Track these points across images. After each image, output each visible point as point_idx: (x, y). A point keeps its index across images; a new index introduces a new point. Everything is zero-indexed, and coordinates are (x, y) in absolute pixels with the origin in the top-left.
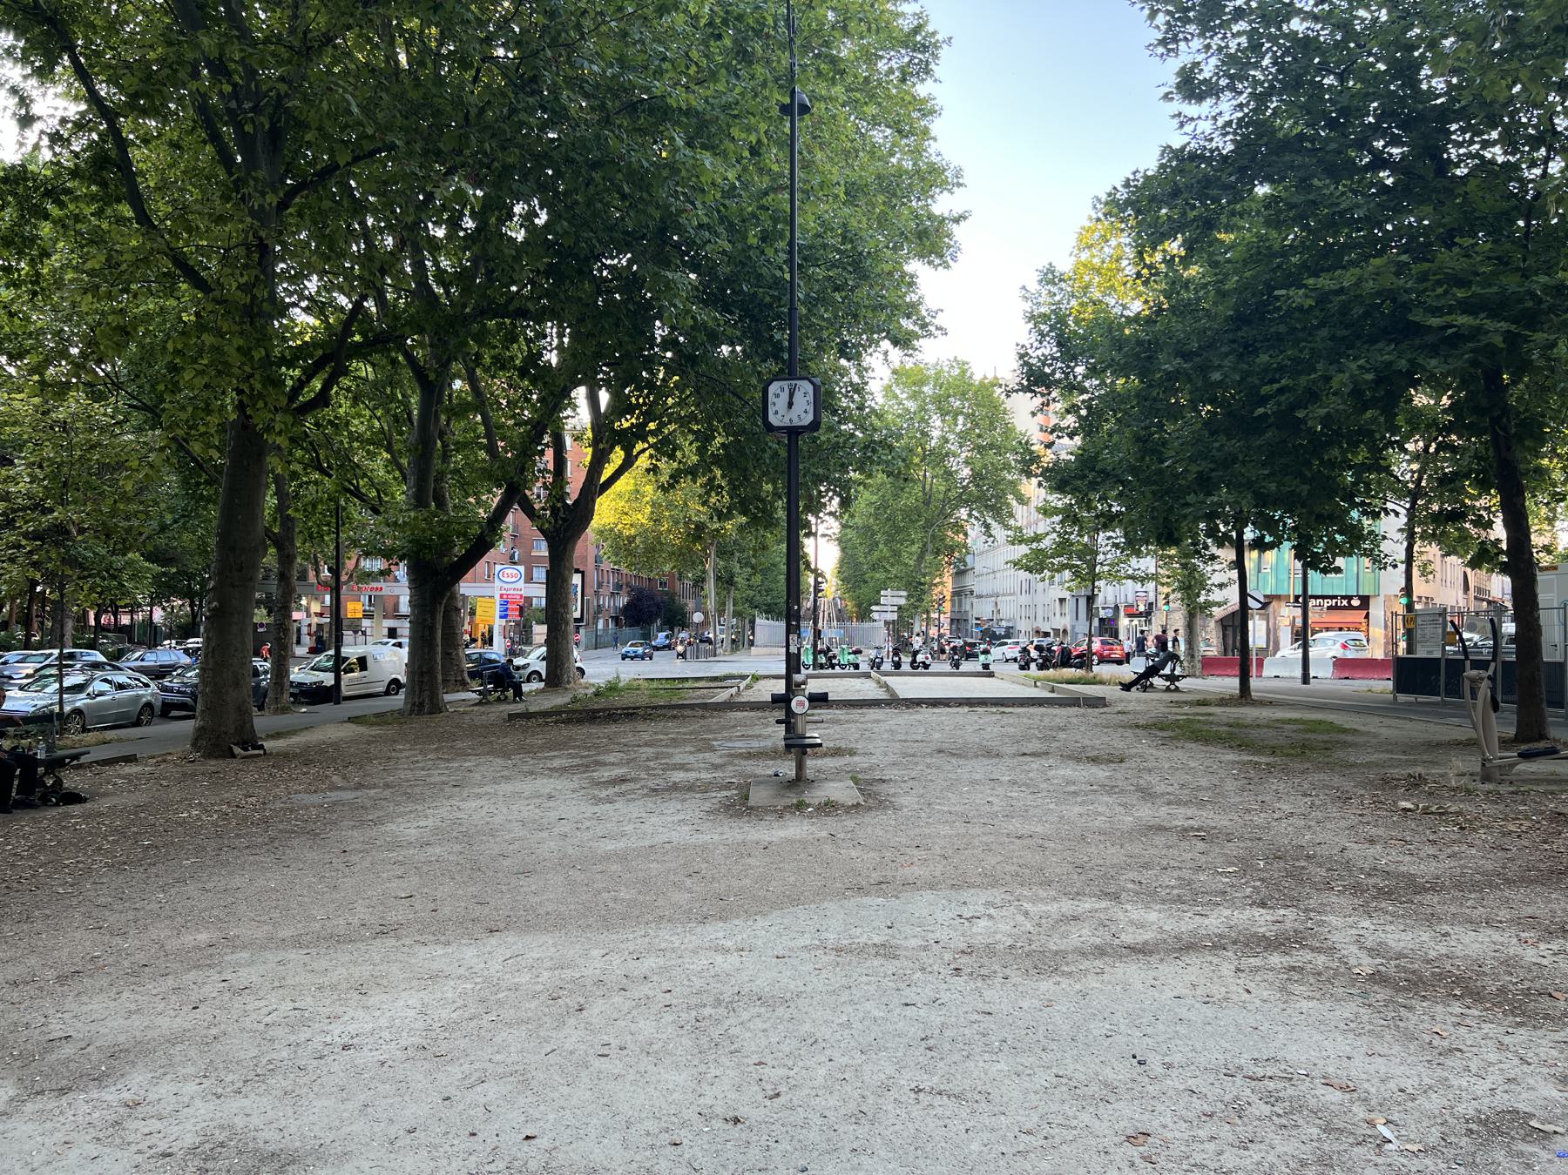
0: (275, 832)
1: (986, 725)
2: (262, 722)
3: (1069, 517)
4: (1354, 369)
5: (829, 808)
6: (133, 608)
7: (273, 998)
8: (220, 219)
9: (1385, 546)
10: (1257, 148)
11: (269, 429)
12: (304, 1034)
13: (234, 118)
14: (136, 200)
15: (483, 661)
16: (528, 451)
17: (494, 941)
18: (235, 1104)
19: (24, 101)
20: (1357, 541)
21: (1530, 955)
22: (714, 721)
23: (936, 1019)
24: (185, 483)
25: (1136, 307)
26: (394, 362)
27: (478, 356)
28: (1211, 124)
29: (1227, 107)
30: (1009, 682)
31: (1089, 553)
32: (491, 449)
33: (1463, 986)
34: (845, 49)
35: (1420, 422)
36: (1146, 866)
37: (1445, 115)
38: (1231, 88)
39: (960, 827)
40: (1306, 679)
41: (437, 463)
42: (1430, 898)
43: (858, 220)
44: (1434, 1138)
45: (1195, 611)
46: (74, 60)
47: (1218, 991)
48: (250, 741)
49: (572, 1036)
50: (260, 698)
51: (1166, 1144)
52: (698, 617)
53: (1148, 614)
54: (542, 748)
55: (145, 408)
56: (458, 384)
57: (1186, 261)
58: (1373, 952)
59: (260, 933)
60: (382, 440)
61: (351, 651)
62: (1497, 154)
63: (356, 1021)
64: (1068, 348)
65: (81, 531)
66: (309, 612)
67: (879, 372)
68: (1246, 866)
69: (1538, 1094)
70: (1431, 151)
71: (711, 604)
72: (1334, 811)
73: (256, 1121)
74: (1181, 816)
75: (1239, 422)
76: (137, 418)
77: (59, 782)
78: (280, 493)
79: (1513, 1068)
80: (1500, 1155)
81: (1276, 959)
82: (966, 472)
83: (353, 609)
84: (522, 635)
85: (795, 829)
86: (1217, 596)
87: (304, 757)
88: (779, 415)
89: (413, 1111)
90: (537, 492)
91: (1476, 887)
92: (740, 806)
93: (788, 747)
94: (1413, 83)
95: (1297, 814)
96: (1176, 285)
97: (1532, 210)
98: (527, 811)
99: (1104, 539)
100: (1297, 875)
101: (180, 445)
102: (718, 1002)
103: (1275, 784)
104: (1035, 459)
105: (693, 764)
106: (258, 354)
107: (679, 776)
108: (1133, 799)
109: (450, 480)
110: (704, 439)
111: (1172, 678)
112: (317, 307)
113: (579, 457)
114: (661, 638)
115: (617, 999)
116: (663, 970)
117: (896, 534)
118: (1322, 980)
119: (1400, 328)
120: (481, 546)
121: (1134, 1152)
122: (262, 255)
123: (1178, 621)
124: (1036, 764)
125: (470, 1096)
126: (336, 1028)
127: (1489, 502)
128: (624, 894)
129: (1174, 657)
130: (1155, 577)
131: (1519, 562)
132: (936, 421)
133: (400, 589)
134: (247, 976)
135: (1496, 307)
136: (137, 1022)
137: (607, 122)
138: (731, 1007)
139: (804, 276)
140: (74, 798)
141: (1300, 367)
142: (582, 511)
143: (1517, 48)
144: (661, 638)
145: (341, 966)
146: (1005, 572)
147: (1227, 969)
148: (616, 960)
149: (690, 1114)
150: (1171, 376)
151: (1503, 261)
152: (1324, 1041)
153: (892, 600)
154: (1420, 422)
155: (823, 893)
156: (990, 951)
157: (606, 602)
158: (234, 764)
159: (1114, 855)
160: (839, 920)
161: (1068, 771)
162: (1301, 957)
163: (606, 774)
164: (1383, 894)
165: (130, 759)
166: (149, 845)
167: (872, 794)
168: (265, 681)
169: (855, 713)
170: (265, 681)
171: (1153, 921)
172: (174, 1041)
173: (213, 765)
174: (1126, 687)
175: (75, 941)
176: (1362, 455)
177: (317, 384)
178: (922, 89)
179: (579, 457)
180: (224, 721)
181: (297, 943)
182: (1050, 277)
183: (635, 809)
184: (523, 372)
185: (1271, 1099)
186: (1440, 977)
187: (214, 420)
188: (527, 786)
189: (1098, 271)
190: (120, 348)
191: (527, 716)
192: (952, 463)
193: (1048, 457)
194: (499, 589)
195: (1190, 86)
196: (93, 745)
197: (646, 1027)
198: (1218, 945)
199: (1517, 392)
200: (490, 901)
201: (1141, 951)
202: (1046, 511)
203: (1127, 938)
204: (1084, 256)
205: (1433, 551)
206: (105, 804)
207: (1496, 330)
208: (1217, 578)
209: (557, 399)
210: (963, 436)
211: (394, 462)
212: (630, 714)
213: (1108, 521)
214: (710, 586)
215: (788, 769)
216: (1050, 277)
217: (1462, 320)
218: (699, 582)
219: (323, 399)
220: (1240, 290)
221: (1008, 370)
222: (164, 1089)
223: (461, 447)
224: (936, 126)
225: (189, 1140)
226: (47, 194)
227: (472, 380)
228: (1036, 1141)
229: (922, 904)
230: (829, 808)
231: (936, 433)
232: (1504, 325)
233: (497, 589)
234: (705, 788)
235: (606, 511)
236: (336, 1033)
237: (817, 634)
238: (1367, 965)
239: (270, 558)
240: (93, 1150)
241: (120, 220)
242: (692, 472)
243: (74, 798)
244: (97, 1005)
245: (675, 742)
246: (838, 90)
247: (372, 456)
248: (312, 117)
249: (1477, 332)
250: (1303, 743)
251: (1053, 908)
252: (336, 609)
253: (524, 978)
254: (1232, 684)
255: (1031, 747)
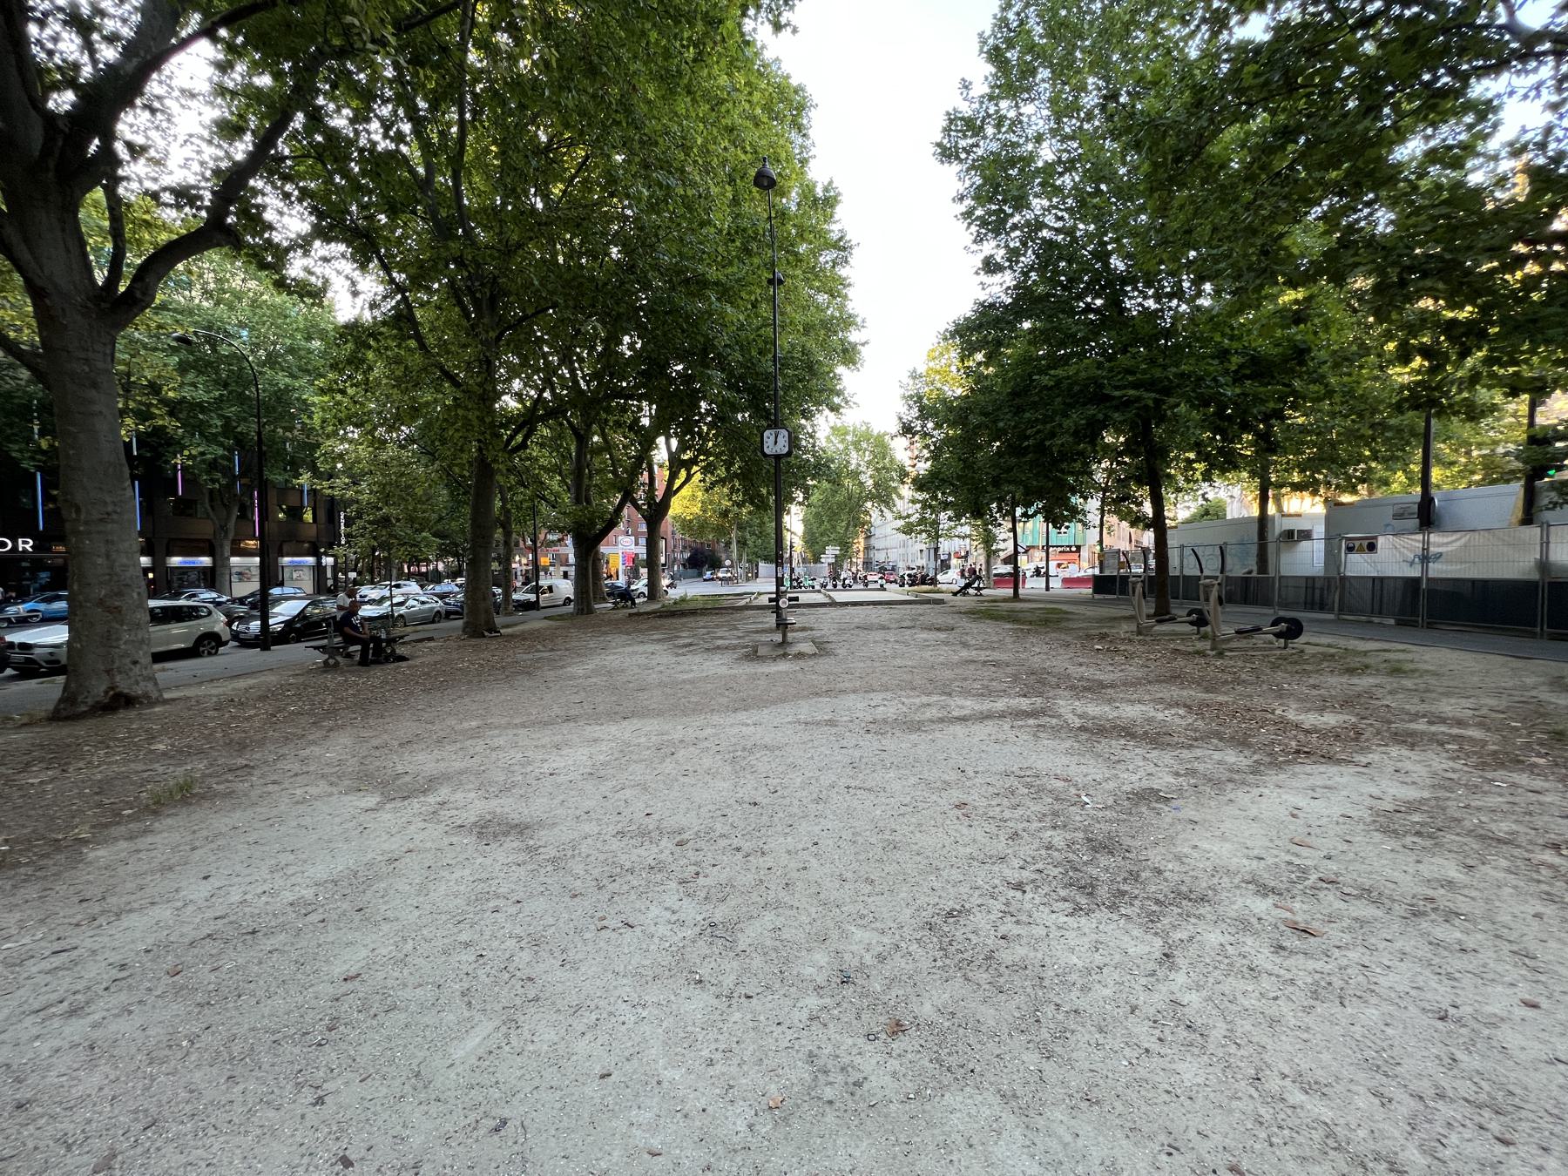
0: (510, 673)
1: (883, 614)
2: (499, 620)
3: (925, 505)
4: (1076, 418)
5: (800, 656)
6: (428, 561)
7: (512, 752)
8: (465, 346)
9: (1090, 517)
10: (1025, 301)
11: (495, 461)
12: (530, 768)
13: (471, 292)
14: (419, 338)
15: (613, 587)
16: (634, 471)
17: (626, 723)
18: (494, 803)
19: (354, 284)
20: (1075, 513)
21: (1160, 716)
22: (738, 615)
23: (857, 754)
24: (452, 493)
25: (959, 392)
26: (561, 424)
27: (606, 421)
28: (999, 288)
29: (1009, 278)
30: (893, 593)
31: (936, 523)
32: (615, 472)
33: (1127, 732)
34: (803, 249)
35: (1110, 451)
36: (965, 679)
37: (1124, 281)
38: (1010, 267)
39: (869, 663)
40: (1047, 588)
41: (586, 481)
42: (1109, 691)
43: (811, 345)
44: (1110, 802)
45: (990, 554)
46: (380, 259)
47: (1002, 737)
48: (493, 629)
49: (669, 767)
50: (497, 607)
51: (975, 808)
52: (728, 563)
53: (966, 557)
54: (648, 630)
55: (428, 453)
56: (596, 439)
57: (987, 365)
58: (1080, 717)
59: (503, 721)
60: (556, 469)
61: (544, 582)
62: (1151, 304)
63: (556, 762)
64: (925, 413)
65: (398, 520)
66: (520, 563)
67: (822, 429)
68: (1016, 678)
69: (1163, 780)
70: (1115, 303)
71: (735, 556)
72: (1061, 651)
73: (506, 810)
74: (983, 655)
75: (1012, 449)
76: (424, 460)
77: (393, 650)
78: (503, 499)
79: (1151, 768)
80: (1144, 809)
81: (1031, 722)
82: (870, 482)
83: (544, 561)
84: (634, 574)
85: (783, 666)
86: (1002, 546)
87: (523, 637)
88: (770, 448)
89: (589, 804)
90: (640, 495)
91: (1133, 685)
92: (753, 655)
93: (778, 625)
94: (1106, 264)
95: (1040, 653)
96: (980, 378)
97: (1168, 333)
98: (642, 660)
99: (943, 516)
100: (1043, 683)
101: (447, 471)
102: (744, 749)
103: (1032, 639)
104: (907, 475)
105: (726, 636)
106: (488, 420)
107: (720, 642)
108: (958, 648)
109: (593, 491)
110: (729, 464)
111: (978, 589)
112: (519, 396)
113: (662, 475)
114: (708, 574)
115: (692, 749)
116: (715, 735)
117: (834, 516)
118: (1055, 731)
119: (1102, 399)
120: (611, 524)
121: (959, 813)
122: (488, 367)
123: (982, 560)
124: (908, 632)
125: (617, 796)
126: (546, 766)
127: (1143, 492)
128: (693, 699)
129: (979, 578)
130: (969, 536)
131: (1158, 523)
132: (854, 454)
133: (569, 550)
134: (501, 741)
135: (1150, 385)
136: (442, 764)
137: (673, 289)
138: (751, 752)
139: (782, 374)
140: (402, 659)
141: (1047, 419)
142: (664, 505)
143: (1164, 243)
144: (708, 574)
145: (546, 736)
146: (891, 535)
147: (1006, 727)
148: (690, 730)
149: (732, 802)
150: (978, 426)
151: (1152, 362)
152: (1053, 758)
153: (831, 552)
154: (1110, 451)
155: (797, 697)
156: (885, 721)
157: (678, 556)
158: (485, 641)
159: (948, 674)
160: (805, 710)
161: (924, 635)
162: (1044, 720)
163: (681, 642)
164: (1085, 689)
165: (430, 639)
166: (442, 680)
167: (822, 649)
168: (499, 599)
169: (813, 610)
170: (499, 599)
171: (970, 705)
172: (461, 773)
173: (474, 641)
174: (955, 594)
175: (406, 726)
176: (1078, 465)
177: (519, 438)
178: (843, 272)
179: (662, 475)
180: (479, 619)
181: (523, 725)
182: (914, 376)
183: (698, 659)
184: (631, 428)
185: (1029, 786)
186: (1114, 728)
187: (465, 456)
188: (641, 648)
189: (938, 372)
190: (414, 418)
191: (639, 614)
192: (863, 478)
193: (913, 473)
194: (621, 549)
195: (990, 266)
196: (411, 633)
197: (707, 762)
198: (1002, 715)
199: (1158, 431)
200: (624, 703)
201: (963, 719)
202: (914, 502)
203: (955, 714)
204: (931, 364)
205: (1112, 519)
206: (418, 662)
207: (1149, 397)
208: (1001, 537)
209: (648, 444)
210: (869, 463)
211: (563, 481)
212: (693, 613)
213: (946, 506)
214: (734, 546)
215: (778, 638)
216: (914, 376)
217: (1131, 392)
218: (728, 544)
219: (523, 446)
220: (1014, 378)
221: (895, 427)
222: (459, 796)
223: (599, 472)
224: (850, 292)
225: (473, 819)
226: (370, 335)
227: (603, 435)
228: (909, 809)
229: (850, 700)
230: (800, 656)
231: (854, 462)
232: (1153, 395)
233: (620, 550)
234: (735, 647)
235: (677, 507)
236: (546, 768)
237: (792, 570)
238: (1078, 723)
239: (498, 534)
240: (422, 825)
241: (410, 350)
242: (722, 481)
243: (402, 659)
244: (421, 757)
245: (717, 626)
246: (798, 272)
247: (551, 478)
248: (513, 288)
249: (1138, 399)
250: (1048, 619)
251: (917, 701)
252: (535, 562)
253: (643, 740)
254: (1010, 592)
255: (905, 624)
